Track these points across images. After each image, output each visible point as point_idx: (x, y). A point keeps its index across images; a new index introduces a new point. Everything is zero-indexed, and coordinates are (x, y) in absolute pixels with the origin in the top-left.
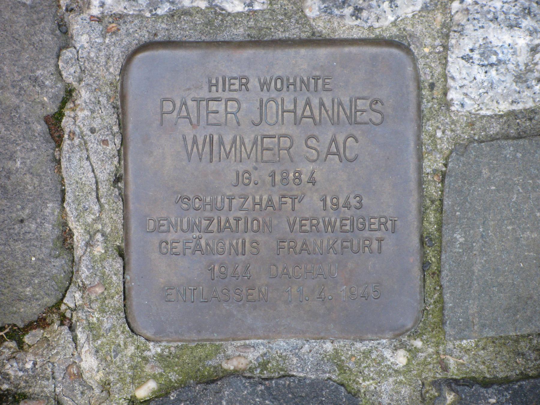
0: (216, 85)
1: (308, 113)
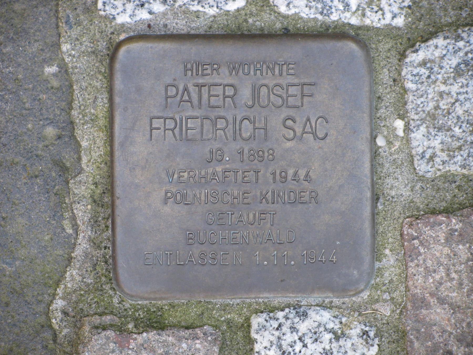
0: (192, 70)
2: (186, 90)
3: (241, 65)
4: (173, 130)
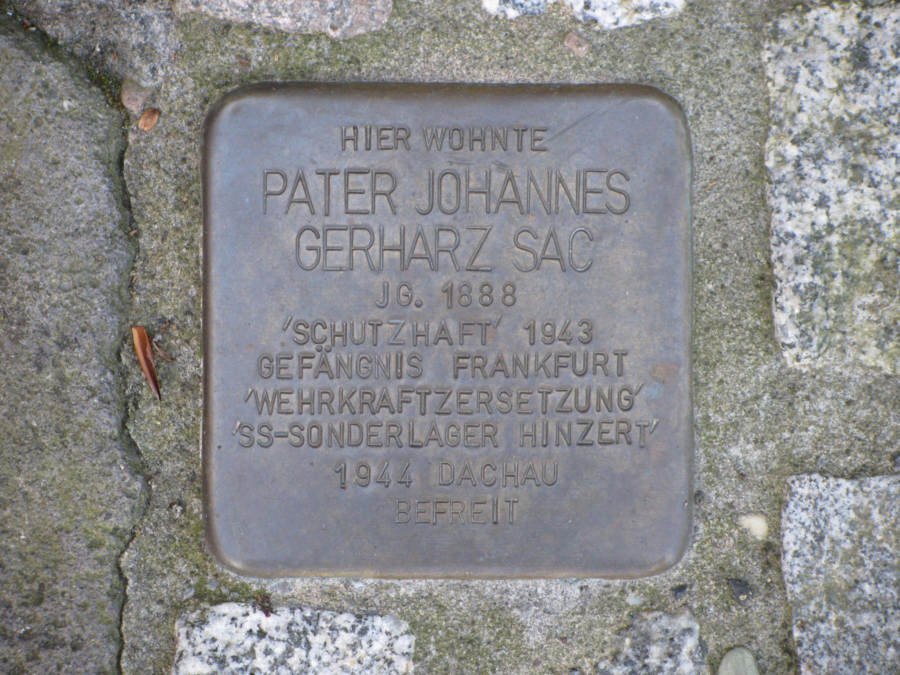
0: (355, 140)
1: (509, 194)
2: (300, 179)
3: (447, 132)
4: (387, 194)
